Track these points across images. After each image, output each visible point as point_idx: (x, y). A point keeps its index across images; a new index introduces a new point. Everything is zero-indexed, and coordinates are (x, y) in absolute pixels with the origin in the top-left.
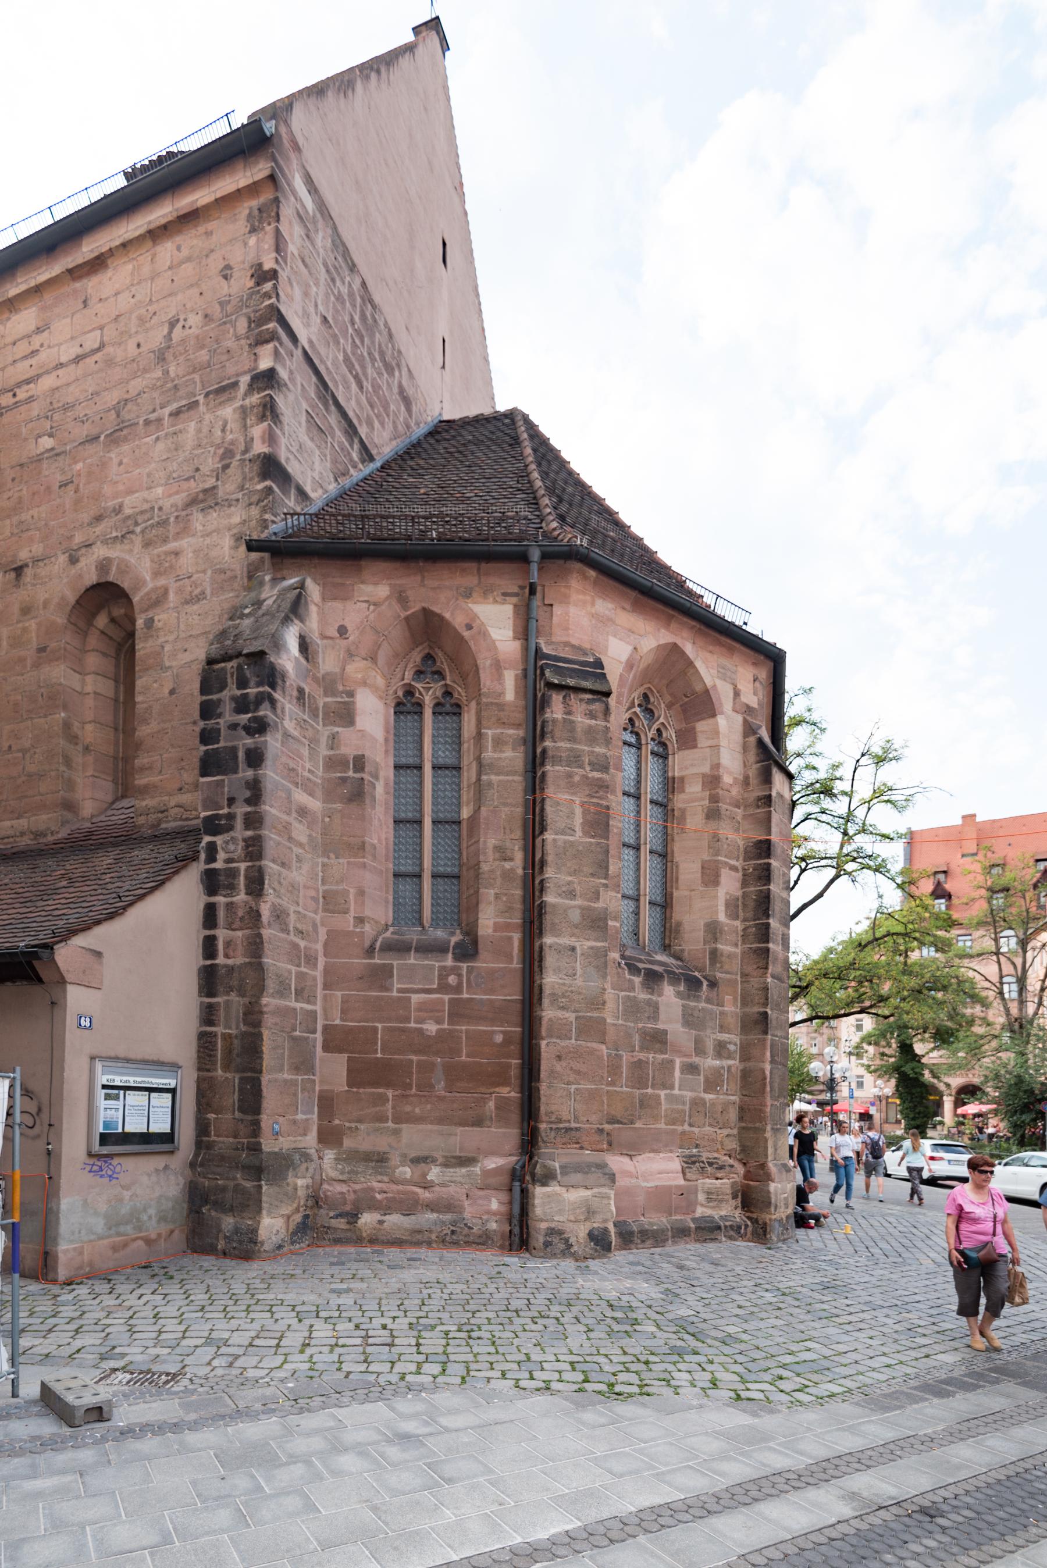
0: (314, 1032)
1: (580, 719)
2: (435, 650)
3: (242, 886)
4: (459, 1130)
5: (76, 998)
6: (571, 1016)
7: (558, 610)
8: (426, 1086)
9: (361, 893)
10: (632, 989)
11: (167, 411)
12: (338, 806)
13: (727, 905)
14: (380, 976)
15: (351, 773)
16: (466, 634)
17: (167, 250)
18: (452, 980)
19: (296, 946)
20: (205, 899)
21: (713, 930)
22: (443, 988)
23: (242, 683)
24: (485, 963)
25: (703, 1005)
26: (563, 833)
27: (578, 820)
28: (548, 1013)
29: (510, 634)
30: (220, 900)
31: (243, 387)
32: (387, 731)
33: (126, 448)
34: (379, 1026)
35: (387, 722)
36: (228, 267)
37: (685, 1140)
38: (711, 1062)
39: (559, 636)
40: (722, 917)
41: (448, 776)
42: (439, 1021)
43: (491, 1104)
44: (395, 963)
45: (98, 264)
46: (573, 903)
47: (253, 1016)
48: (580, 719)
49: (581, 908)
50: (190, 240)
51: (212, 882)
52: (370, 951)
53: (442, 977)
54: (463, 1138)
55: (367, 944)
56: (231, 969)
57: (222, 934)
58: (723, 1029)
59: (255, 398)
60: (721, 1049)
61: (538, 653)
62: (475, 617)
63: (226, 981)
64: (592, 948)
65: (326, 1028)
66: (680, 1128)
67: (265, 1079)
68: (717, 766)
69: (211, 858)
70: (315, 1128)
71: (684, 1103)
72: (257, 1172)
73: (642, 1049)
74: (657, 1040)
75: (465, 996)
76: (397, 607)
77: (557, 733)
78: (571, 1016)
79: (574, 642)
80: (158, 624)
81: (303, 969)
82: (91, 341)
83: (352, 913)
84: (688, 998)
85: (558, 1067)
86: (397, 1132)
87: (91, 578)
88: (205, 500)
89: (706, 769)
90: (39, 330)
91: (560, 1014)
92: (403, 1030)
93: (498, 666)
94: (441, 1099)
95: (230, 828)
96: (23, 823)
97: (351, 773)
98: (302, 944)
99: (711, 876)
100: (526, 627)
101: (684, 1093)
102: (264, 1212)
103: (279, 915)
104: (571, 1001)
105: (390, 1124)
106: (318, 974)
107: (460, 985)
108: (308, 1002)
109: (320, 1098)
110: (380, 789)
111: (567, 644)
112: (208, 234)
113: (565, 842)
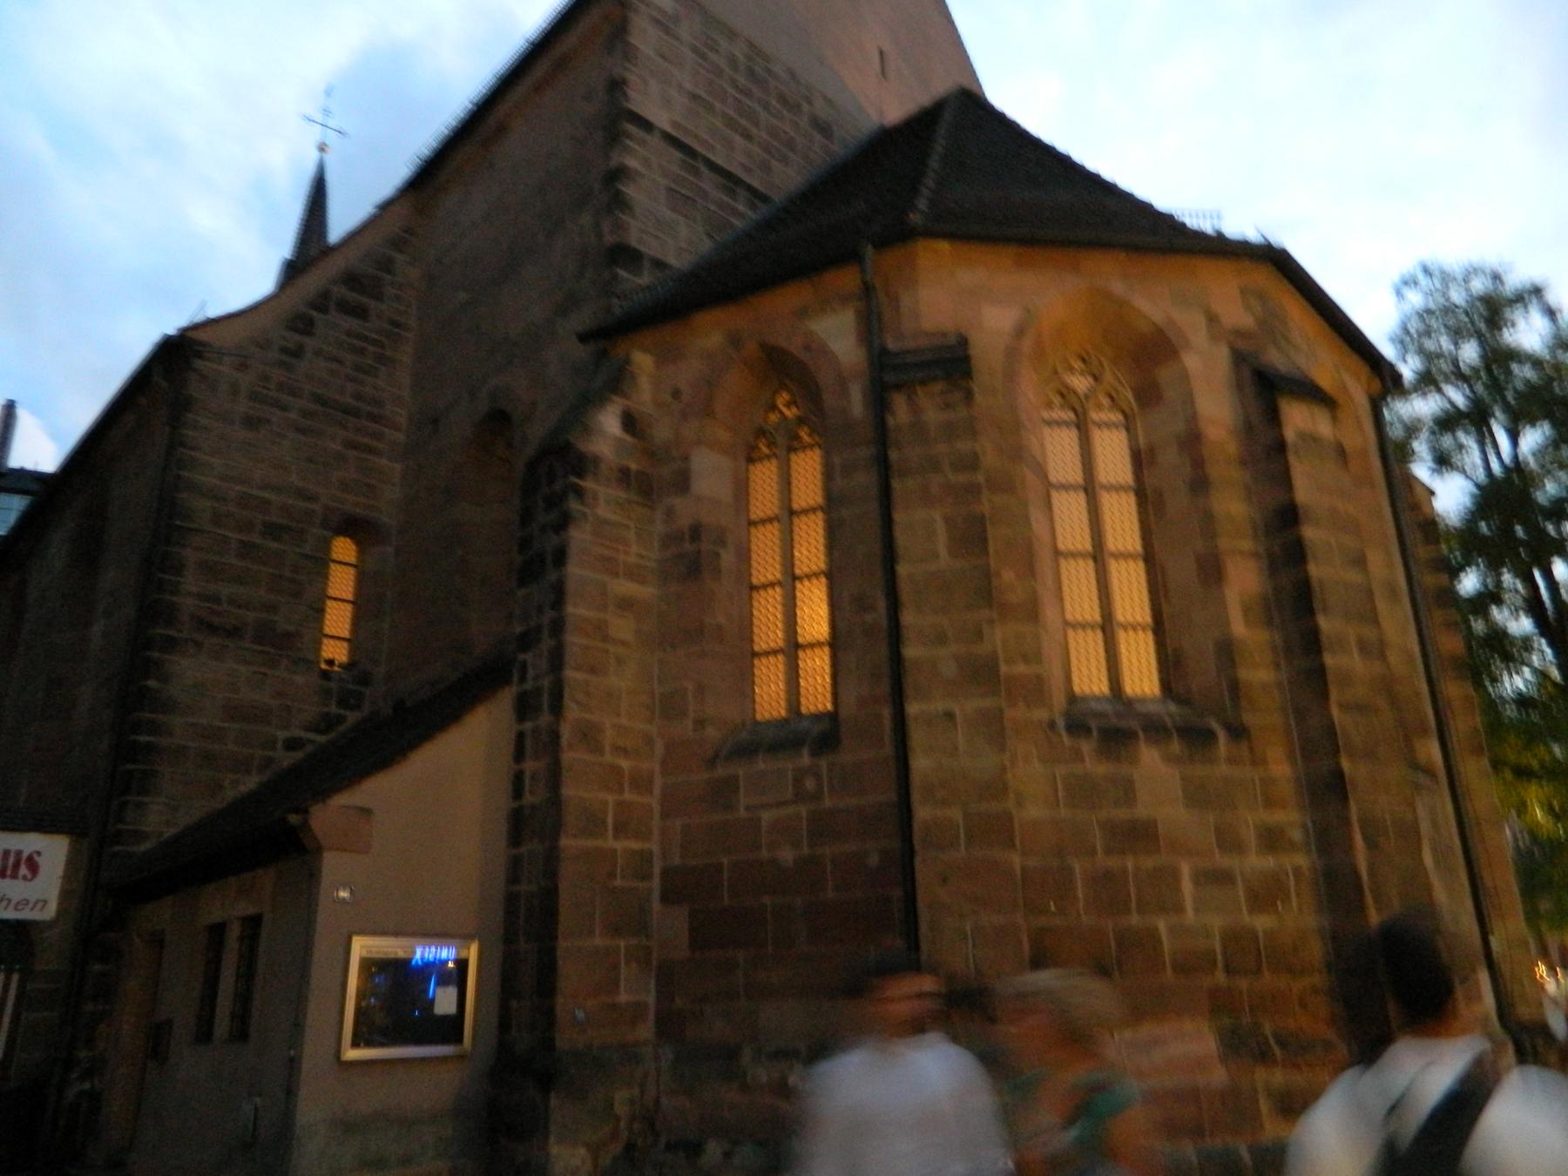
1: (933, 415)
2: (783, 368)
3: (545, 706)
5: (332, 864)
6: (956, 814)
9: (701, 689)
10: (1078, 756)
13: (1246, 610)
14: (722, 793)
18: (810, 784)
19: (616, 771)
22: (800, 796)
28: (923, 813)
30: (528, 726)
34: (725, 861)
37: (1220, 1005)
38: (1256, 862)
44: (741, 772)
47: (552, 859)
48: (933, 415)
51: (524, 707)
52: (712, 763)
53: (798, 781)
56: (533, 807)
58: (1270, 803)
60: (1272, 840)
61: (884, 352)
63: (532, 822)
65: (665, 873)
67: (563, 945)
68: (1193, 418)
69: (523, 679)
72: (547, 1081)
73: (1109, 851)
74: (1140, 835)
78: (956, 814)
81: (628, 796)
98: (625, 764)
100: (870, 326)
102: (552, 1139)
103: (589, 736)
106: (654, 801)
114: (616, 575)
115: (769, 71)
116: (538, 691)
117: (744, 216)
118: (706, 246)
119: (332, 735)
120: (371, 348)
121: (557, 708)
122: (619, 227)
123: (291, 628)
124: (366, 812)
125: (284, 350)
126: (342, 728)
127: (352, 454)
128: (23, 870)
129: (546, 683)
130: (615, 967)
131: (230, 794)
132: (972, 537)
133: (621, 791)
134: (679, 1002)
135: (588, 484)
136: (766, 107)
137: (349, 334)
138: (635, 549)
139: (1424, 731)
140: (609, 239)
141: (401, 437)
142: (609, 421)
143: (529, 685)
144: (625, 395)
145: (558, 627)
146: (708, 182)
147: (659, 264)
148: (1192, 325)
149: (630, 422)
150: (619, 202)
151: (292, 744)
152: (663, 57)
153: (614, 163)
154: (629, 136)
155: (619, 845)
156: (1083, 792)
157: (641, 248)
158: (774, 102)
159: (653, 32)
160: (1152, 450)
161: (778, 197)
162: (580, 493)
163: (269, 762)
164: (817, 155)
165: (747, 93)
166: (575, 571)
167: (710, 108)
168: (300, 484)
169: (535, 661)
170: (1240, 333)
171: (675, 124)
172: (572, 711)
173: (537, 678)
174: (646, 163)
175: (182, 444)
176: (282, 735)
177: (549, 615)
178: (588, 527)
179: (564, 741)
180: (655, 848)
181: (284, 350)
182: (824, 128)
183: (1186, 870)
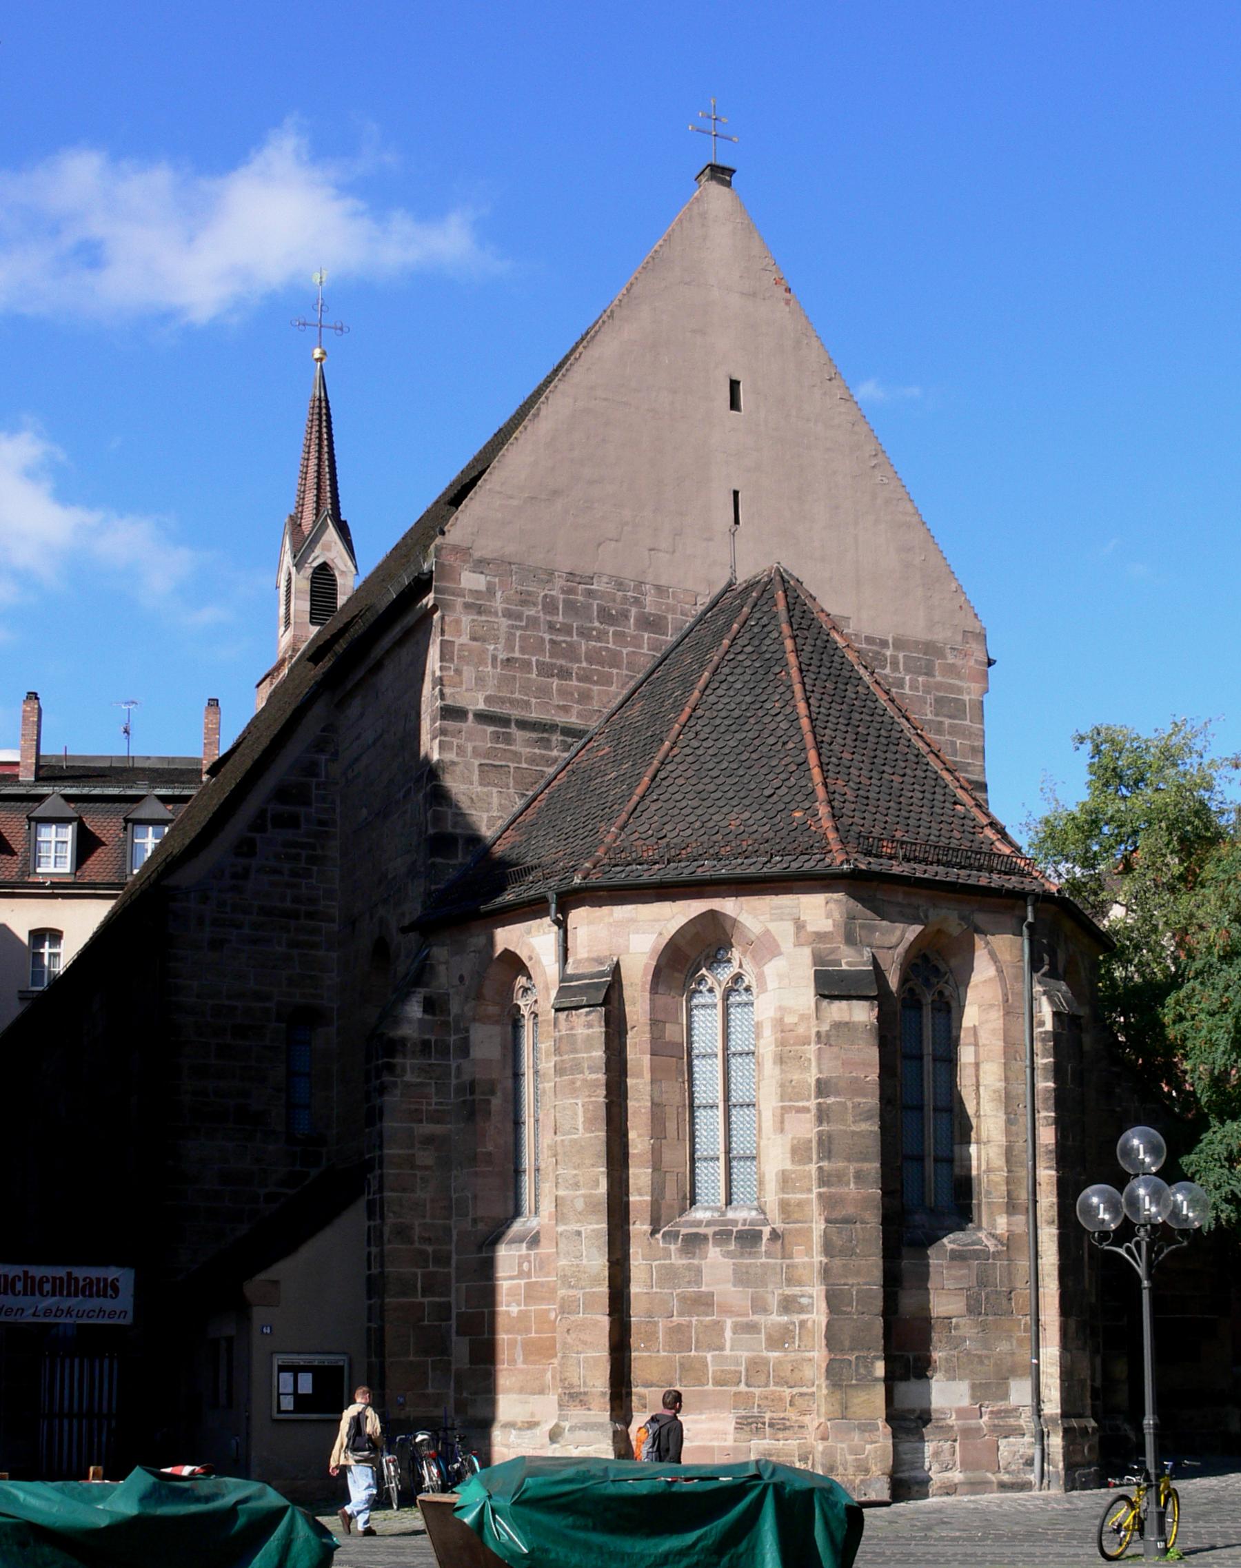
0: (449, 1319)
5: (259, 1315)
12: (462, 1125)
19: (423, 1253)
22: (521, 1274)
25: (764, 1260)
26: (569, 1133)
27: (581, 1119)
37: (740, 1400)
42: (519, 1305)
45: (379, 666)
46: (578, 1193)
49: (584, 1196)
53: (520, 1265)
60: (788, 1305)
64: (593, 1230)
65: (458, 1315)
70: (452, 1401)
71: (738, 1364)
73: (681, 1314)
74: (703, 1302)
75: (534, 1279)
78: (579, 1294)
81: (431, 1269)
83: (470, 1217)
84: (742, 1255)
85: (569, 1339)
91: (571, 1292)
94: (521, 1371)
98: (430, 1249)
101: (739, 1353)
103: (403, 1232)
104: (579, 1279)
107: (530, 1269)
108: (441, 1295)
113: (571, 1141)
114: (421, 1121)
115: (590, 593)
124: (276, 1283)
125: (235, 876)
128: (110, 1292)
133: (427, 1267)
134: (465, 1395)
135: (398, 1060)
138: (434, 1100)
141: (335, 927)
142: (414, 1010)
143: (371, 1197)
144: (427, 986)
146: (521, 741)
149: (430, 1005)
155: (426, 1300)
158: (597, 624)
159: (466, 620)
162: (390, 1068)
165: (566, 629)
166: (390, 1124)
170: (820, 936)
171: (488, 700)
172: (391, 1220)
178: (398, 1092)
179: (386, 1237)
180: (852, 1168)
182: (652, 623)
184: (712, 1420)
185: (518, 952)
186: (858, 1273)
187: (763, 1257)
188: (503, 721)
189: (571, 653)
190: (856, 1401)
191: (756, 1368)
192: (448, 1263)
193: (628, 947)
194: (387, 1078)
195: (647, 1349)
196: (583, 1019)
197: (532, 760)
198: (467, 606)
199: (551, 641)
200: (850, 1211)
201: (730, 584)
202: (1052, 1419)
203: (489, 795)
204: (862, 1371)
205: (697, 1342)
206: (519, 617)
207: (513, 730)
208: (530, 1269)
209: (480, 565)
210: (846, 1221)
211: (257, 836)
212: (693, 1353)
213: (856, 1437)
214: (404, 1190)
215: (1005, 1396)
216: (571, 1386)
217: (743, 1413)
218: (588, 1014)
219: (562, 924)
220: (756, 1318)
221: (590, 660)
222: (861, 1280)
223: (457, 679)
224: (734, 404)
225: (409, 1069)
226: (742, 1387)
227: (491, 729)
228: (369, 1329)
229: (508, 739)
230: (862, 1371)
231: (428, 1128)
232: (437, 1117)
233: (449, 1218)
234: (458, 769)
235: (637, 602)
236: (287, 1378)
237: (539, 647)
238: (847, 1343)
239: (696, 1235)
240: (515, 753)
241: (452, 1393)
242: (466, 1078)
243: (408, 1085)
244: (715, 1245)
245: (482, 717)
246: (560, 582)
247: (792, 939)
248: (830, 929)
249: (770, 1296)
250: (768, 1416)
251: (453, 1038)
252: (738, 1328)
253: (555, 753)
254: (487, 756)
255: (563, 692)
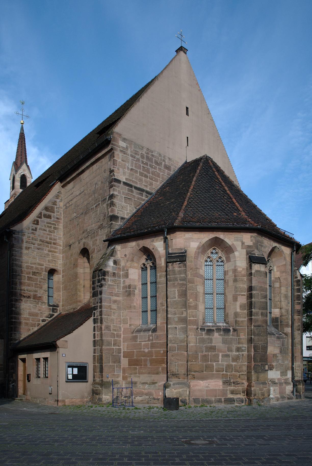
2: (148, 253)
4: (153, 375)
6: (176, 345)
7: (174, 241)
8: (146, 365)
9: (131, 318)
11: (95, 206)
12: (125, 298)
15: (128, 289)
16: (152, 251)
17: (95, 166)
20: (94, 325)
21: (236, 315)
22: (149, 340)
23: (99, 277)
24: (159, 333)
25: (231, 337)
27: (177, 295)
29: (163, 249)
30: (96, 325)
31: (107, 199)
32: (139, 276)
33: (88, 215)
35: (139, 274)
36: (105, 170)
39: (174, 247)
40: (238, 310)
41: (154, 284)
42: (148, 349)
43: (160, 369)
50: (98, 164)
51: (95, 321)
53: (149, 337)
54: (155, 377)
55: (132, 331)
56: (98, 341)
57: (96, 333)
59: (109, 202)
60: (238, 350)
62: (154, 246)
65: (123, 352)
66: (222, 373)
68: (235, 266)
69: (94, 316)
70: (122, 376)
73: (206, 352)
74: (213, 348)
76: (137, 247)
77: (171, 274)
78: (176, 345)
79: (178, 247)
80: (93, 257)
82: (82, 190)
84: (225, 335)
86: (139, 377)
87: (82, 247)
88: (101, 227)
89: (233, 268)
90: (73, 188)
92: (140, 351)
93: (160, 257)
95: (97, 309)
96: (71, 307)
97: (128, 289)
98: (115, 333)
99: (235, 299)
100: (167, 247)
103: (108, 328)
105: (138, 375)
107: (153, 339)
109: (123, 369)
110: (137, 291)
111: (176, 249)
112: (102, 162)
115: (153, 155)
116: (97, 319)
117: (145, 198)
118: (135, 210)
119: (51, 318)
120: (53, 226)
121: (101, 323)
122: (113, 210)
123: (40, 295)
125: (33, 230)
126: (53, 317)
127: (50, 253)
129: (99, 317)
130: (114, 368)
131: (32, 332)
132: (184, 294)
135: (106, 277)
136: (151, 166)
137: (47, 223)
139: (287, 326)
140: (111, 214)
141: (62, 248)
142: (111, 263)
145: (101, 307)
147: (123, 218)
148: (238, 245)
149: (115, 262)
150: (112, 204)
151: (43, 321)
152: (123, 161)
153: (111, 193)
154: (115, 186)
155: (114, 347)
156: (202, 341)
157: (119, 215)
158: (154, 164)
159: (121, 154)
160: (227, 271)
161: (154, 192)
162: (104, 279)
163: (39, 324)
164: (165, 176)
165: (146, 164)
167: (136, 172)
168: (40, 262)
169: (97, 312)
170: (249, 247)
171: (126, 179)
173: (97, 316)
174: (119, 192)
175: (13, 256)
176: (41, 319)
177: (99, 304)
178: (107, 286)
179: (103, 329)
180: (260, 311)
181: (33, 230)
182: (167, 168)
183: (220, 354)
184: (215, 382)
185: (148, 247)
186: (261, 341)
187: (231, 335)
188: (131, 186)
189: (148, 171)
190: (261, 376)
191: (229, 367)
192: (120, 337)
193: (190, 246)
194: (103, 282)
195: (195, 361)
196: (178, 265)
197: (138, 199)
198: (121, 151)
199: (143, 166)
200: (259, 323)
201: (186, 161)
202: (299, 381)
203: (127, 206)
204: (262, 368)
205: (211, 359)
206: (135, 157)
207: (133, 189)
208: (153, 339)
209: (124, 140)
210: (259, 326)
211: (39, 219)
212: (209, 363)
213: (261, 386)
214: (108, 315)
215: (287, 375)
216: (173, 372)
217: (225, 380)
218: (179, 264)
219: (165, 239)
220: (229, 353)
221: (152, 174)
222: (262, 343)
223: (118, 171)
224: (187, 114)
225: (109, 280)
226: (224, 372)
227: (127, 187)
228: (94, 356)
229: (132, 191)
230: (262, 368)
231: (115, 298)
232: (117, 295)
233: (120, 324)
234: (119, 197)
235: (164, 161)
236: (70, 369)
237: (139, 167)
238: (259, 360)
239: (210, 329)
240: (134, 196)
241: (121, 374)
242: (127, 284)
243: (109, 285)
244: (216, 332)
245: (125, 184)
246: (145, 150)
247: (241, 247)
248: (252, 245)
249: (233, 348)
250: (232, 381)
251: (122, 273)
252: (223, 356)
253: (144, 198)
254: (127, 195)
255: (146, 182)
